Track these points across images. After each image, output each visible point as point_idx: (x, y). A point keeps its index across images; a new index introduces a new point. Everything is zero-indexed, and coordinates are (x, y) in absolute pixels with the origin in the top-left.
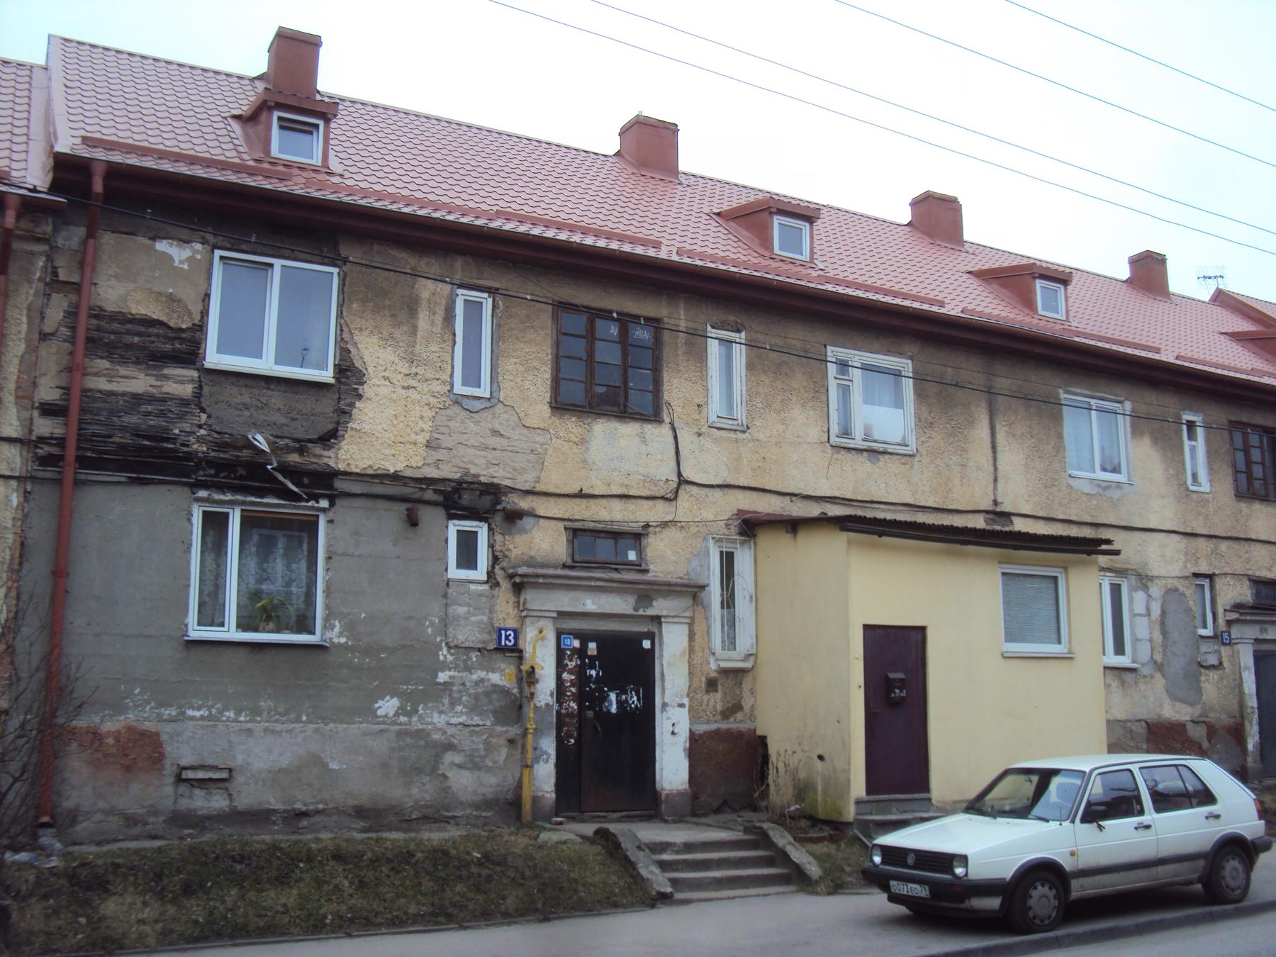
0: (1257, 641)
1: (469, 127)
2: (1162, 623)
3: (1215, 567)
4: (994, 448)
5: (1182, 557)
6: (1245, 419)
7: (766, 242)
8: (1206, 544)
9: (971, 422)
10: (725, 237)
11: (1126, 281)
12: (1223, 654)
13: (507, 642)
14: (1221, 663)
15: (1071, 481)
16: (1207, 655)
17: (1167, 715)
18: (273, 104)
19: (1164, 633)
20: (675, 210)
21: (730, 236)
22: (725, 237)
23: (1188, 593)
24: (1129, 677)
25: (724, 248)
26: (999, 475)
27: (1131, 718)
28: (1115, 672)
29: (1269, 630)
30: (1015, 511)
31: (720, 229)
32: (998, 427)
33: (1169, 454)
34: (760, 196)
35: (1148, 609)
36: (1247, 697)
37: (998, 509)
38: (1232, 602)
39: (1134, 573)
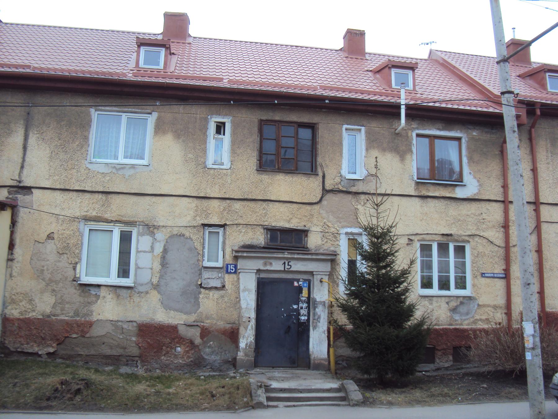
0: (259, 271)
1: (374, 54)
2: (163, 258)
3: (227, 219)
4: (25, 148)
5: (191, 213)
6: (277, 118)
7: (543, 86)
8: (219, 204)
9: (10, 133)
10: (524, 86)
11: (341, 50)
12: (226, 280)
13: (231, 271)
14: (224, 286)
15: (90, 166)
16: (209, 280)
17: (160, 319)
18: (391, 66)
19: (164, 263)
20: (494, 76)
21: (526, 85)
22: (524, 86)
23: (194, 237)
24: (124, 292)
25: (524, 91)
26: (26, 164)
27: (123, 319)
28: (111, 289)
29: (273, 264)
30: (35, 186)
31: (521, 82)
32: (31, 135)
33: (191, 144)
34: (538, 65)
35: (152, 248)
36: (243, 310)
37: (21, 185)
38: (242, 243)
39: (142, 224)
